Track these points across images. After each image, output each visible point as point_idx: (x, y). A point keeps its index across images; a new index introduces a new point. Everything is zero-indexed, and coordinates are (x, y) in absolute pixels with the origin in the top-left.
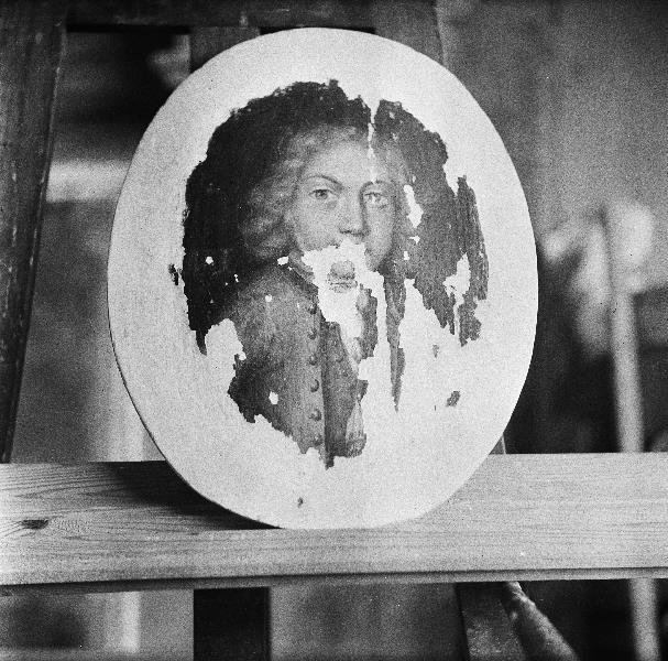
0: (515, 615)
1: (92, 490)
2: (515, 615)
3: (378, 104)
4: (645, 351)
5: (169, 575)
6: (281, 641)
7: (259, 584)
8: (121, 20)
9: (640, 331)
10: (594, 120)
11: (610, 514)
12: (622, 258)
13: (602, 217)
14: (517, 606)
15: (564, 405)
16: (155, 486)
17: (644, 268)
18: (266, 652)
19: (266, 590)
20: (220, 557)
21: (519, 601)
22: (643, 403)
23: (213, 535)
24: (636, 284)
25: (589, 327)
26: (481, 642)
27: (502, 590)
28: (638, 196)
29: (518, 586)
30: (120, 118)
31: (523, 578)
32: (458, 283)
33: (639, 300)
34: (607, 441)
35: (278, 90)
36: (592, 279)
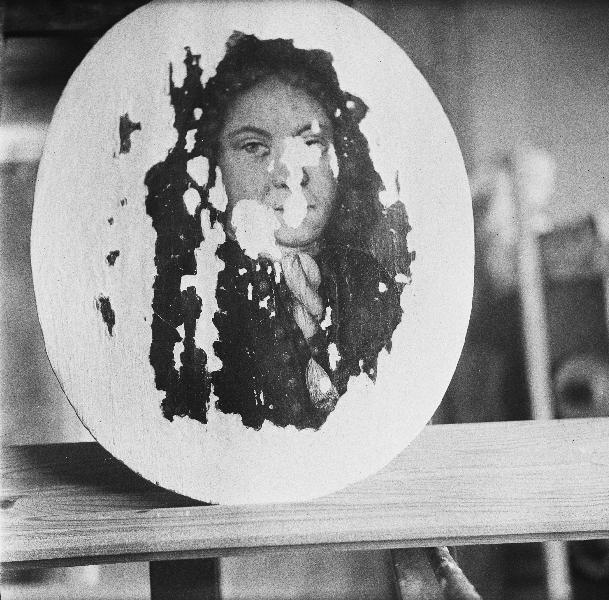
0: (444, 582)
1: (20, 533)
2: (444, 582)
3: (208, 416)
4: (551, 287)
5: (120, 551)
6: (227, 589)
7: (429, 545)
8: (56, 26)
9: (545, 267)
10: (511, 55)
11: (545, 479)
12: (544, 189)
13: (506, 162)
14: (444, 573)
15: (489, 388)
16: (91, 472)
17: (545, 211)
18: (220, 598)
19: (539, 545)
20: (170, 532)
21: (447, 566)
22: (550, 343)
23: (158, 512)
24: (542, 224)
25: (499, 265)
26: (413, 586)
27: (432, 555)
28: (546, 143)
29: (446, 549)
30: (40, 88)
31: (153, 559)
32: (372, 372)
33: (543, 239)
34: (517, 407)
35: (228, 44)
36: (501, 214)
